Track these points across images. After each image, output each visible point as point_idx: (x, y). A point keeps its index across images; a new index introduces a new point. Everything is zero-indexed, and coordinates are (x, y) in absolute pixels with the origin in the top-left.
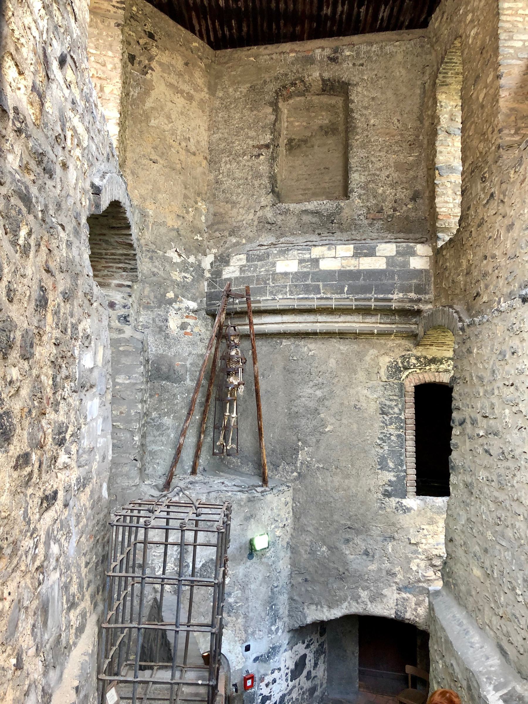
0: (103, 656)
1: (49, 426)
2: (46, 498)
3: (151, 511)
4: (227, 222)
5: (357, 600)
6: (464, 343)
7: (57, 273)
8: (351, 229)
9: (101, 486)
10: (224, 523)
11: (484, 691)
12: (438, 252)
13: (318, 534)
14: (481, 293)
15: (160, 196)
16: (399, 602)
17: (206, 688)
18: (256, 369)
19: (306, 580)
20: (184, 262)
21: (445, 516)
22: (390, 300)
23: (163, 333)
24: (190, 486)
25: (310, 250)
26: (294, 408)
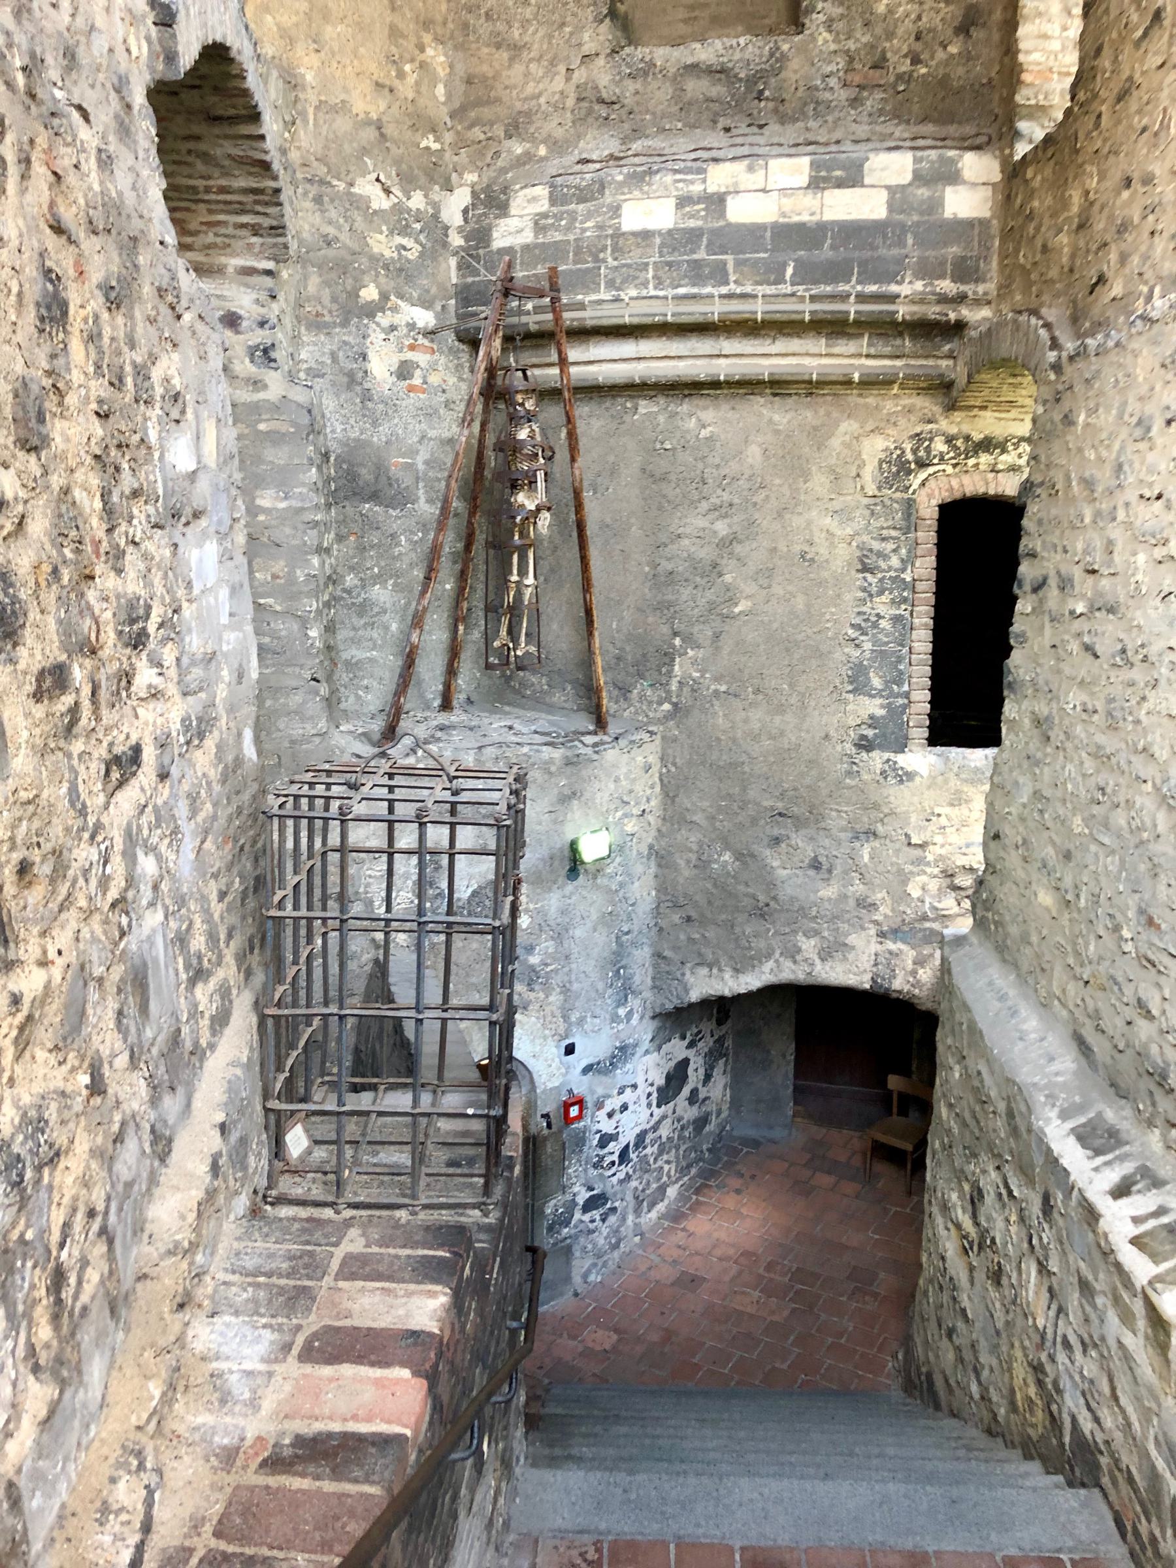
0: (273, 1068)
1: (105, 605)
2: (115, 761)
3: (354, 787)
4: (498, 100)
5: (793, 957)
6: (1058, 400)
7: (81, 234)
8: (803, 113)
9: (239, 735)
10: (509, 807)
11: (1038, 1120)
12: (1014, 172)
13: (715, 829)
14: (1110, 274)
15: (330, 32)
16: (881, 959)
17: (484, 1121)
18: (577, 472)
19: (689, 919)
20: (398, 209)
21: (987, 787)
22: (892, 298)
23: (358, 389)
24: (439, 734)
25: (704, 171)
26: (664, 563)
